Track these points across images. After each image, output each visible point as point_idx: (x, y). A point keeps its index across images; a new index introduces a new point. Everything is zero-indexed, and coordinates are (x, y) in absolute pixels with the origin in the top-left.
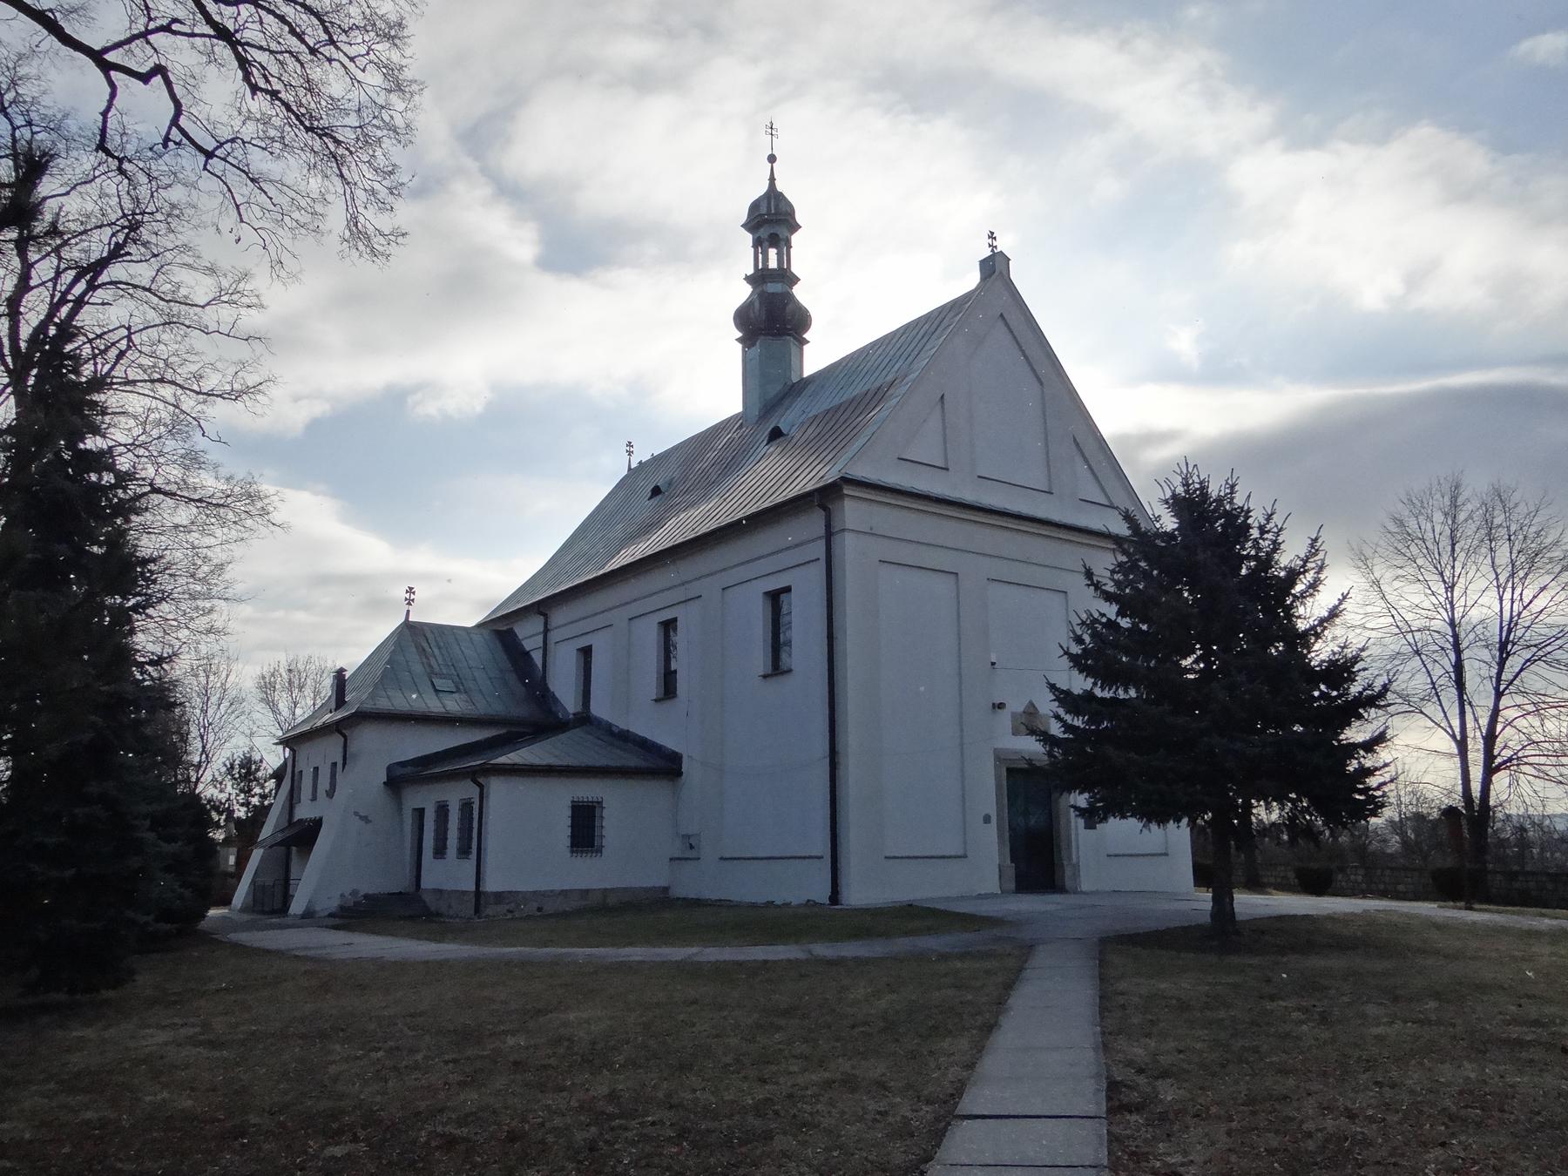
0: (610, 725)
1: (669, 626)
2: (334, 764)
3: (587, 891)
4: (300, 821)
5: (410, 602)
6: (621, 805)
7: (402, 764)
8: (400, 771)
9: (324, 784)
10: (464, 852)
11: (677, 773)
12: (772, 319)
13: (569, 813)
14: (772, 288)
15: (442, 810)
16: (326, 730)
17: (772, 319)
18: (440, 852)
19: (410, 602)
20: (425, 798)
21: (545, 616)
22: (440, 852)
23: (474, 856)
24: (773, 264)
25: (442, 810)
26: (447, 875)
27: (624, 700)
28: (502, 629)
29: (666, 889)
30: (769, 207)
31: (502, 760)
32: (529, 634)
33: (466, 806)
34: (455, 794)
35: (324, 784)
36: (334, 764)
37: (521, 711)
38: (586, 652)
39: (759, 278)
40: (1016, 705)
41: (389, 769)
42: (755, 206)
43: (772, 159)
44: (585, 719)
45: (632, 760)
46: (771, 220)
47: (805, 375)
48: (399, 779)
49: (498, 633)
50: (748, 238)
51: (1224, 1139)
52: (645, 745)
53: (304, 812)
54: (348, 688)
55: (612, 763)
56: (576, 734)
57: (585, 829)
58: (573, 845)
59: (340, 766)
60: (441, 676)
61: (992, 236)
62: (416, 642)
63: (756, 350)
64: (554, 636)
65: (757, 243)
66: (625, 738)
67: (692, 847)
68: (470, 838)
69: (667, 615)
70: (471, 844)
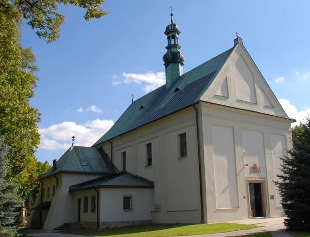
0: (132, 174)
1: (149, 146)
2: (54, 187)
3: (128, 221)
4: (44, 202)
5: (73, 140)
6: (138, 197)
7: (73, 186)
8: (72, 188)
9: (51, 192)
10: (93, 211)
11: (153, 187)
12: (172, 59)
13: (123, 199)
14: (173, 50)
15: (86, 199)
16: (51, 176)
17: (172, 59)
18: (86, 211)
19: (73, 140)
20: (81, 195)
21: (112, 144)
22: (86, 211)
23: (96, 212)
24: (173, 43)
25: (86, 199)
26: (88, 217)
27: (136, 165)
28: (99, 147)
29: (151, 221)
30: (172, 28)
31: (103, 184)
32: (107, 149)
33: (93, 198)
34: (90, 194)
35: (51, 192)
36: (54, 187)
37: (105, 170)
38: (124, 154)
39: (168, 48)
40: (251, 165)
41: (70, 188)
42: (168, 28)
43: (172, 15)
44: (124, 173)
45: (145, 184)
46: (171, 32)
47: (181, 75)
48: (72, 191)
49: (98, 149)
50: (166, 36)
51: (3, 168)
52: (143, 179)
53: (45, 200)
54: (57, 165)
55: (133, 185)
56: (122, 177)
57: (127, 203)
58: (124, 208)
59: (56, 188)
60: (84, 161)
61: (237, 33)
62: (77, 151)
63: (169, 67)
64: (114, 149)
65: (169, 38)
66: (136, 177)
67: (158, 208)
68: (95, 207)
69: (148, 142)
70: (96, 208)
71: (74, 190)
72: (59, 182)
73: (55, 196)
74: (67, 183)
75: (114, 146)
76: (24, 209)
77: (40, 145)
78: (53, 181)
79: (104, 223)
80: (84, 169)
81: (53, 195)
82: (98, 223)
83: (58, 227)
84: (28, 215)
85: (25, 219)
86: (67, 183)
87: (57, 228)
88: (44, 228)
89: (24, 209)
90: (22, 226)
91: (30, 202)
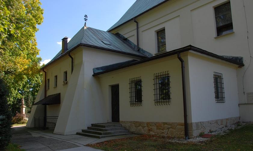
4: (49, 96)
7: (98, 69)
19: (86, 20)
20: (110, 80)
32: (129, 33)
53: (51, 92)
64: (141, 30)
71: (99, 74)
72: (76, 62)
73: (69, 84)
74: (90, 63)
75: (140, 25)
76: (24, 106)
77: (40, 52)
78: (66, 65)
79: (197, 124)
80: (141, 27)
81: (66, 82)
82: (187, 126)
83: (83, 131)
84: (28, 113)
85: (25, 116)
86: (90, 63)
87: (80, 131)
88: (56, 130)
89: (24, 106)
90: (23, 123)
91: (29, 100)
